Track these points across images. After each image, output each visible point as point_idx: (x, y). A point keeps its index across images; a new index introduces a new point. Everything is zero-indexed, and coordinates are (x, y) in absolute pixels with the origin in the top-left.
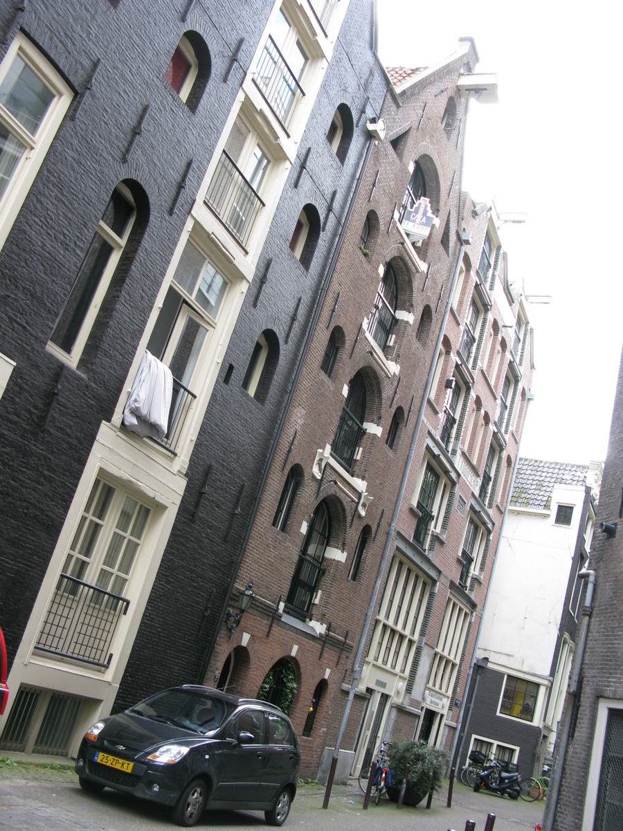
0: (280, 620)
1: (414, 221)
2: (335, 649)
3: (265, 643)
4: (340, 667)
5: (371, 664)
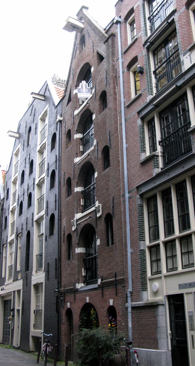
0: (78, 291)
1: (83, 92)
2: (111, 287)
3: (75, 303)
4: (119, 295)
5: (163, 278)
